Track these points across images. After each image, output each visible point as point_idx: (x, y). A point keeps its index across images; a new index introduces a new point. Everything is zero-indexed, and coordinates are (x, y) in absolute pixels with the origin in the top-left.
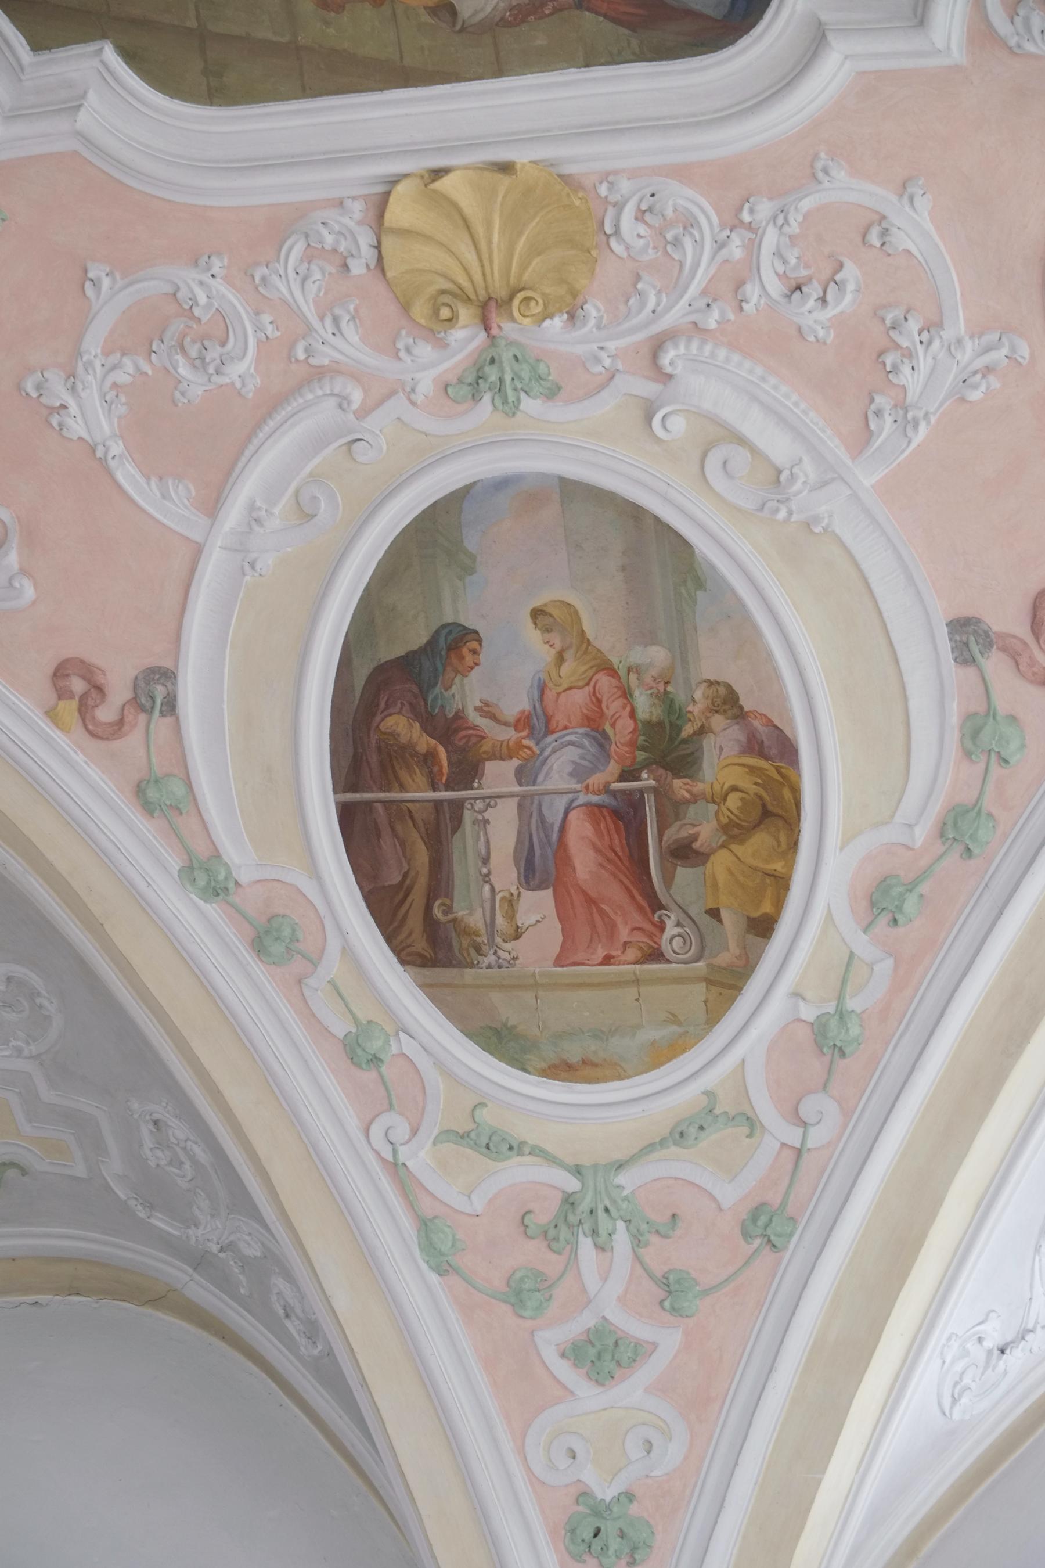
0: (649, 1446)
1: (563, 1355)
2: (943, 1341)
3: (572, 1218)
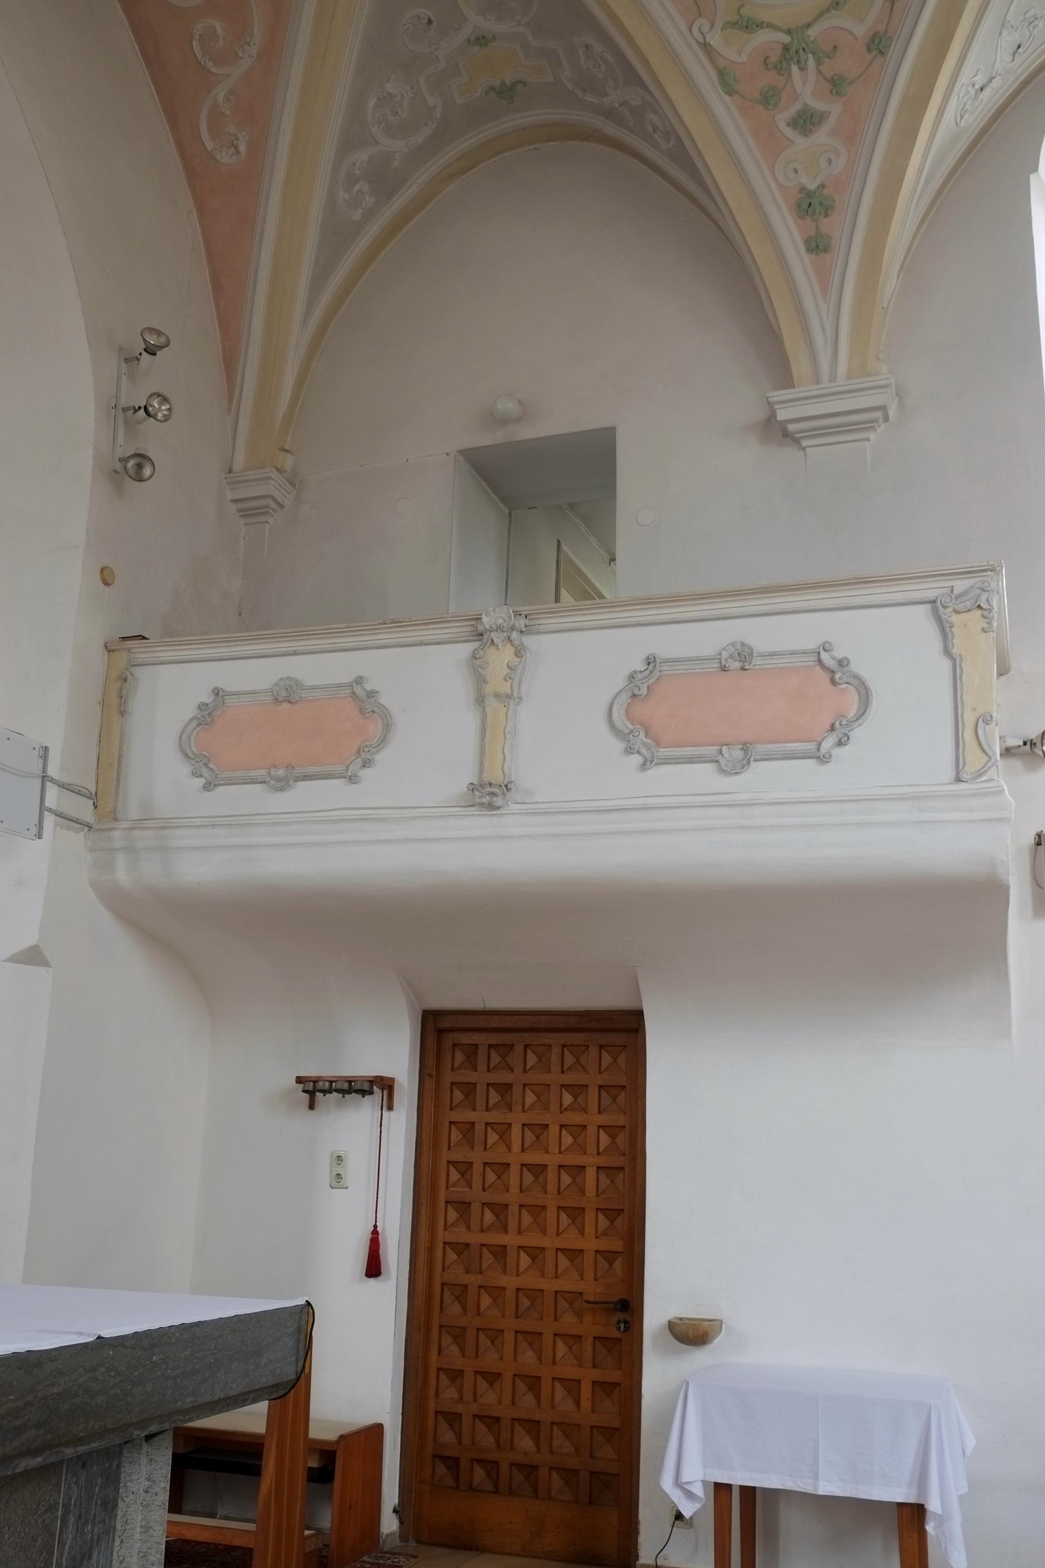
0: (830, 161)
1: (788, 125)
2: (959, 88)
3: (788, 57)
